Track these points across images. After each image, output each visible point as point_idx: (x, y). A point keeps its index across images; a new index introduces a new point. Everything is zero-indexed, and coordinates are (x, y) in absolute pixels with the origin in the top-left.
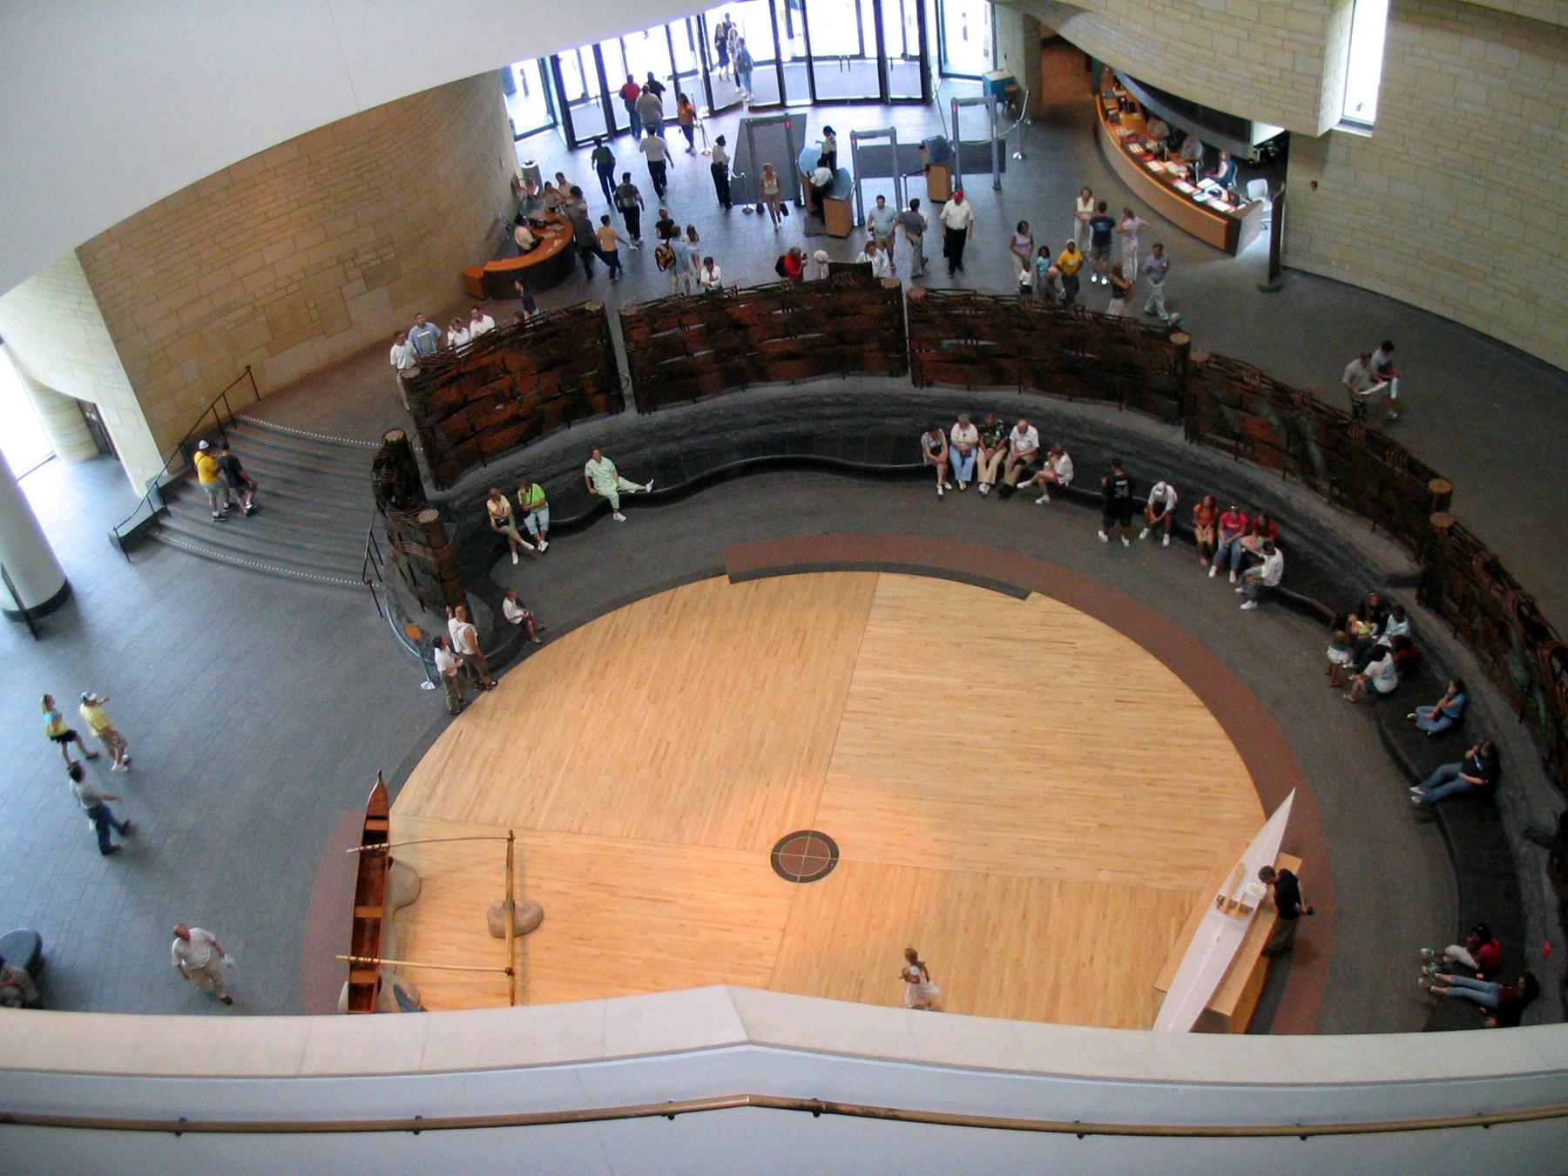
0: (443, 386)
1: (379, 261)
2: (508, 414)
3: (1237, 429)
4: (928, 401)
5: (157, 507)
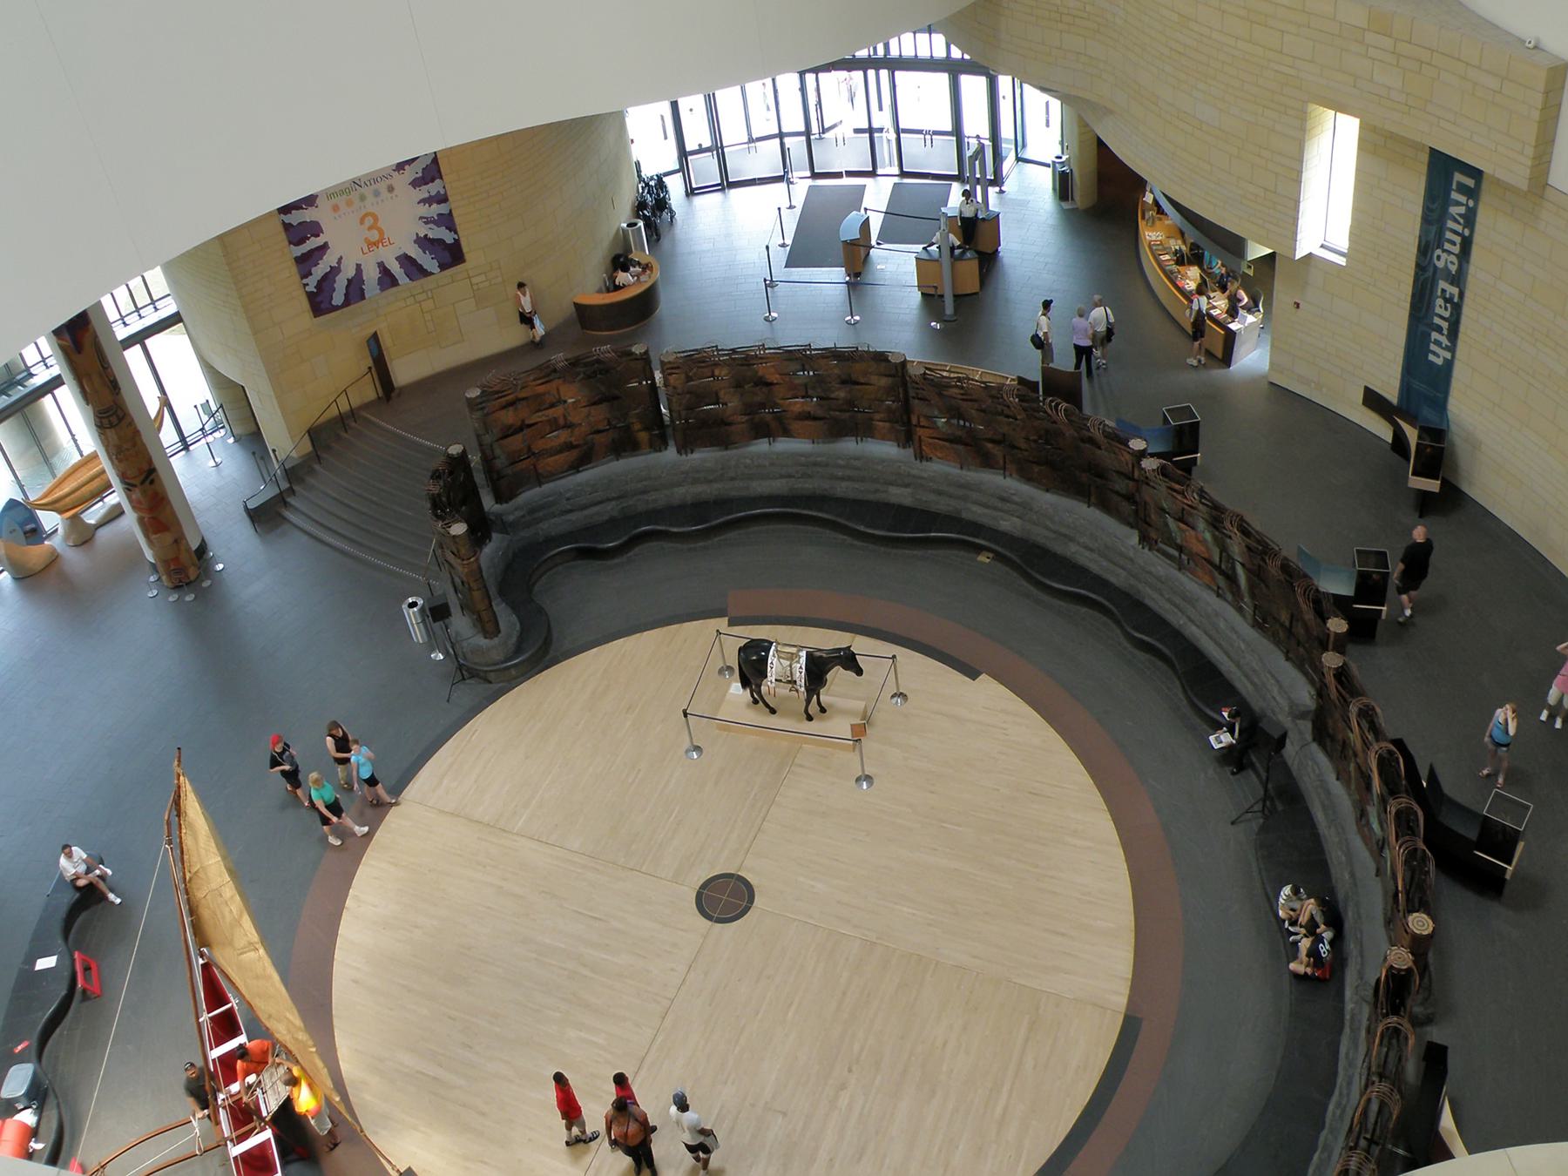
0: (503, 408)
1: (487, 284)
2: (562, 440)
3: (1179, 541)
4: (925, 475)
5: (285, 485)
